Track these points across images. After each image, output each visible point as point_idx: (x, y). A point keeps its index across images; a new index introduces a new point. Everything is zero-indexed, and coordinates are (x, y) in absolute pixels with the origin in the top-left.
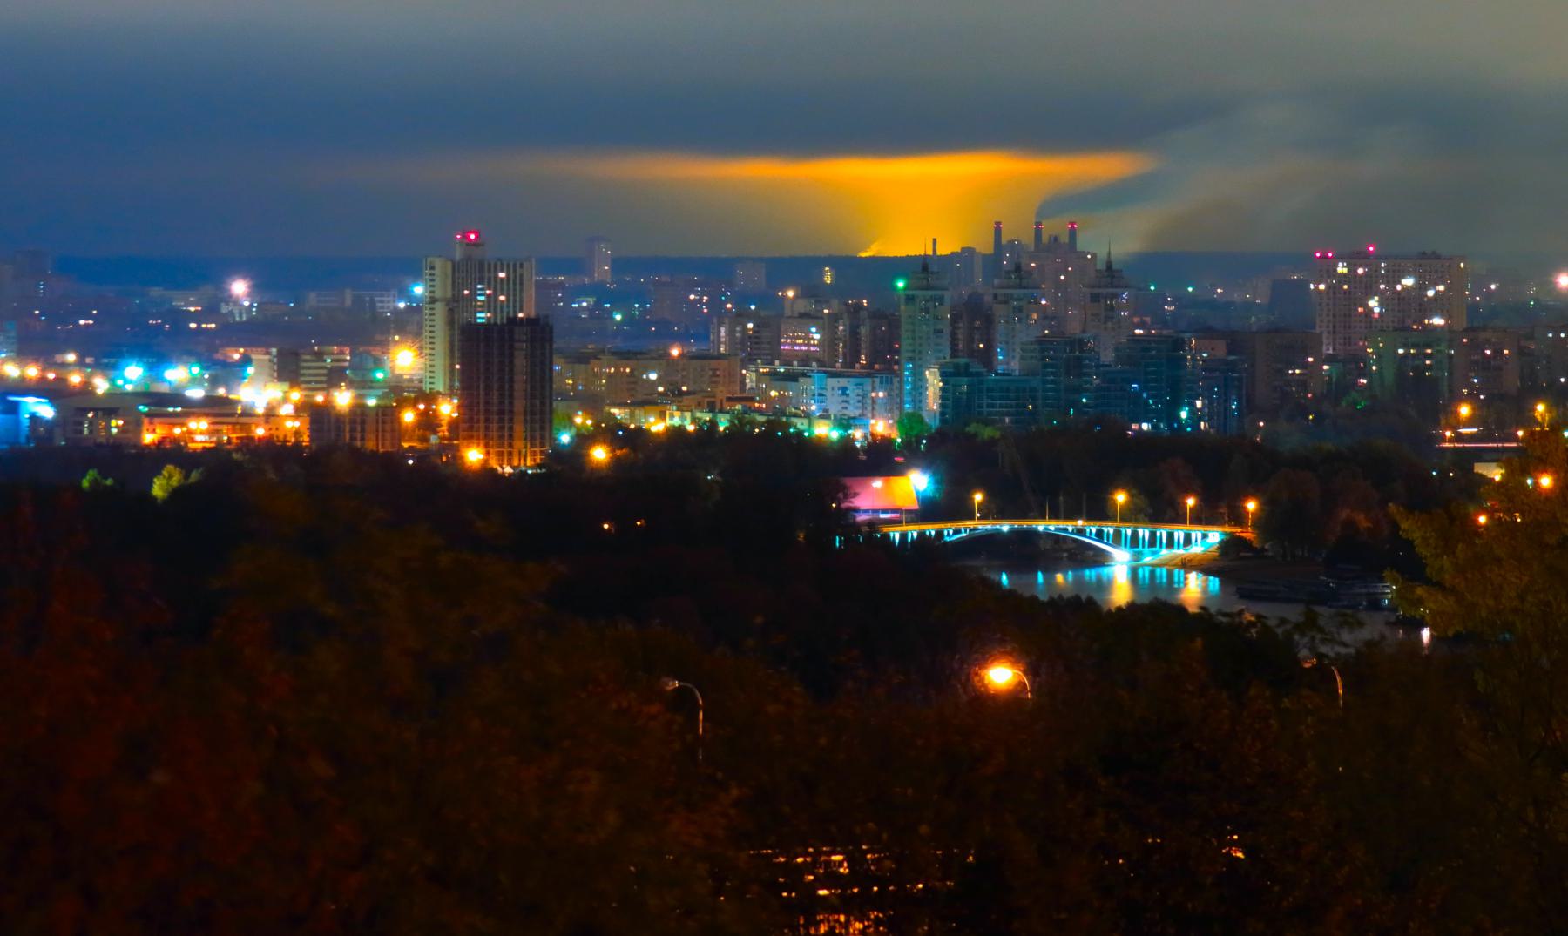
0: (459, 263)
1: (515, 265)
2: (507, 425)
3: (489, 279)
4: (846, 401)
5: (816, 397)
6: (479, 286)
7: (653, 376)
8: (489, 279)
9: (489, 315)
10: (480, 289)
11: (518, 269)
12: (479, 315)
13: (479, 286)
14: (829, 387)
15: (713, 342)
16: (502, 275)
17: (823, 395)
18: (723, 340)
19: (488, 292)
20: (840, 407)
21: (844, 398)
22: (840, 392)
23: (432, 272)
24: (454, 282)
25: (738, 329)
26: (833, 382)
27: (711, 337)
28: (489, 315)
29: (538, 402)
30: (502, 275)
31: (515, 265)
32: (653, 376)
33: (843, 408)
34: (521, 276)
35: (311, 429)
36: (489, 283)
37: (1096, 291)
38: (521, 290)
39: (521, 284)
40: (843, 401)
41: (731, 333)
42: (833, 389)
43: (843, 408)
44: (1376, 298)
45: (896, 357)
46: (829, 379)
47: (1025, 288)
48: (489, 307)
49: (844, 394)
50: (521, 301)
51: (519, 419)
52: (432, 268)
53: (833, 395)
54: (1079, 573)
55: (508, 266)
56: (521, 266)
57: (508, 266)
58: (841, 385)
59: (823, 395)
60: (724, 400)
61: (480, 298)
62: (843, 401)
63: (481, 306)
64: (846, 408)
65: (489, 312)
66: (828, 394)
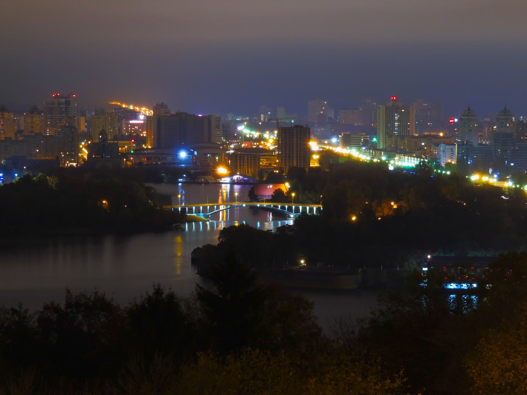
0: (391, 107)
1: (407, 107)
2: (291, 161)
3: (399, 112)
4: (453, 153)
5: (442, 152)
6: (396, 114)
7: (423, 144)
8: (399, 112)
9: (399, 123)
10: (396, 115)
11: (408, 109)
12: (395, 123)
13: (396, 114)
14: (447, 149)
15: (484, 133)
16: (403, 111)
17: (444, 151)
18: (486, 132)
19: (398, 116)
20: (450, 155)
21: (452, 152)
22: (450, 150)
23: (379, 109)
24: (386, 113)
25: (490, 128)
26: (448, 147)
27: (484, 131)
28: (399, 123)
29: (302, 154)
30: (403, 111)
31: (407, 107)
32: (423, 144)
33: (451, 156)
34: (409, 111)
35: (87, 158)
36: (399, 113)
37: (498, 117)
38: (409, 115)
39: (409, 113)
40: (451, 153)
41: (488, 130)
42: (448, 149)
43: (451, 156)
44: (293, 122)
45: (375, 140)
46: (447, 146)
47: (470, 116)
48: (399, 121)
49: (452, 151)
50: (409, 119)
51: (295, 159)
52: (379, 108)
53: (448, 151)
54: (180, 187)
55: (405, 107)
56: (409, 108)
57: (405, 107)
58: (450, 148)
59: (444, 151)
60: (429, 152)
61: (396, 118)
62: (451, 153)
63: (396, 121)
64: (453, 156)
65: (399, 122)
66: (446, 151)
